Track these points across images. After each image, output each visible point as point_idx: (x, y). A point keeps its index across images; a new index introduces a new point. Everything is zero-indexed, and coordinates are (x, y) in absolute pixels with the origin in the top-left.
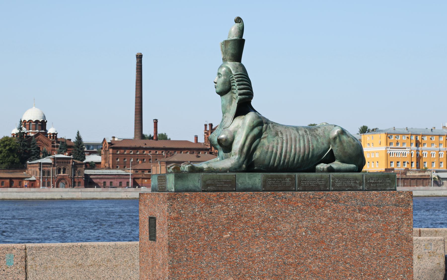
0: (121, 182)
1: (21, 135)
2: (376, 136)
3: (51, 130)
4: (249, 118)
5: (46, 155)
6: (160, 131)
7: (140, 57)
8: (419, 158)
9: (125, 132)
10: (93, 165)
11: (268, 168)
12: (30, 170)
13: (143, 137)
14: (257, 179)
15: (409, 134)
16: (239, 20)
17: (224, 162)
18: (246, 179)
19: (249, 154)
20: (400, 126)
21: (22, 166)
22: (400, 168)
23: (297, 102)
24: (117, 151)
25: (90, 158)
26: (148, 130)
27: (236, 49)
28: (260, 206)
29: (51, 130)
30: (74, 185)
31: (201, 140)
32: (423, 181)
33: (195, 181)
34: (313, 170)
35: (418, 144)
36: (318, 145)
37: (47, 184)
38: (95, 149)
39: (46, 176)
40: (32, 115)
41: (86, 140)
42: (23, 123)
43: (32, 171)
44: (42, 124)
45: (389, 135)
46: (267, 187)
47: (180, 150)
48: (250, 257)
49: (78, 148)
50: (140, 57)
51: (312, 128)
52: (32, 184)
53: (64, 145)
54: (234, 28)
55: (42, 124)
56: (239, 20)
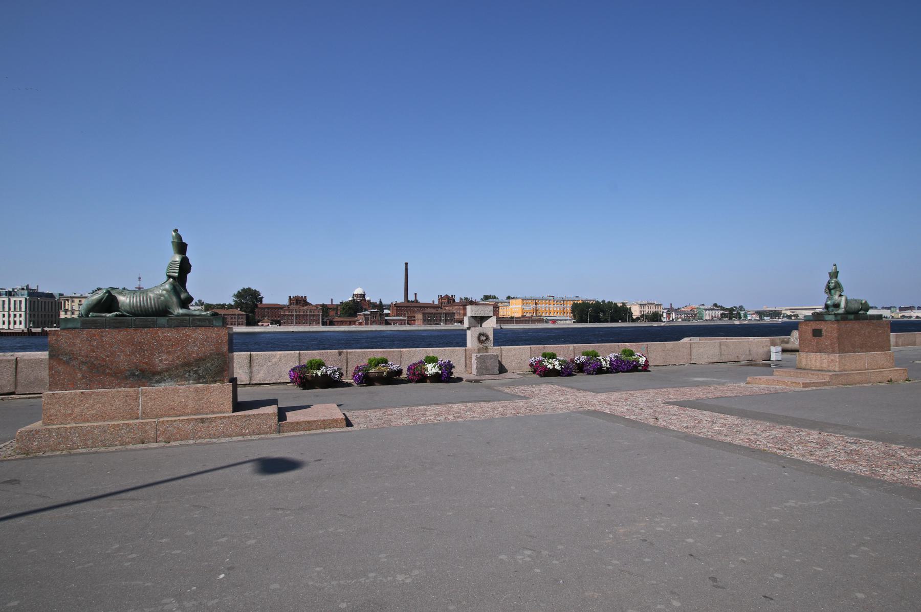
0: (402, 322)
1: (353, 301)
2: (517, 301)
3: (367, 299)
4: (843, 299)
5: (366, 310)
6: (411, 298)
7: (406, 264)
8: (537, 310)
9: (401, 299)
10: (387, 315)
12: (359, 317)
13: (408, 301)
15: (533, 299)
17: (841, 311)
20: (528, 296)
21: (355, 315)
22: (528, 315)
23: (853, 292)
24: (398, 308)
25: (386, 311)
26: (411, 298)
27: (834, 275)
29: (367, 299)
30: (380, 324)
31: (436, 302)
32: (540, 321)
33: (839, 317)
37: (367, 324)
38: (389, 307)
39: (293, 318)
40: (358, 291)
41: (384, 303)
42: (354, 295)
43: (360, 318)
44: (363, 296)
45: (523, 300)
47: (674, 334)
49: (381, 306)
50: (406, 264)
52: (360, 324)
53: (374, 305)
55: (363, 296)
56: (176, 231)
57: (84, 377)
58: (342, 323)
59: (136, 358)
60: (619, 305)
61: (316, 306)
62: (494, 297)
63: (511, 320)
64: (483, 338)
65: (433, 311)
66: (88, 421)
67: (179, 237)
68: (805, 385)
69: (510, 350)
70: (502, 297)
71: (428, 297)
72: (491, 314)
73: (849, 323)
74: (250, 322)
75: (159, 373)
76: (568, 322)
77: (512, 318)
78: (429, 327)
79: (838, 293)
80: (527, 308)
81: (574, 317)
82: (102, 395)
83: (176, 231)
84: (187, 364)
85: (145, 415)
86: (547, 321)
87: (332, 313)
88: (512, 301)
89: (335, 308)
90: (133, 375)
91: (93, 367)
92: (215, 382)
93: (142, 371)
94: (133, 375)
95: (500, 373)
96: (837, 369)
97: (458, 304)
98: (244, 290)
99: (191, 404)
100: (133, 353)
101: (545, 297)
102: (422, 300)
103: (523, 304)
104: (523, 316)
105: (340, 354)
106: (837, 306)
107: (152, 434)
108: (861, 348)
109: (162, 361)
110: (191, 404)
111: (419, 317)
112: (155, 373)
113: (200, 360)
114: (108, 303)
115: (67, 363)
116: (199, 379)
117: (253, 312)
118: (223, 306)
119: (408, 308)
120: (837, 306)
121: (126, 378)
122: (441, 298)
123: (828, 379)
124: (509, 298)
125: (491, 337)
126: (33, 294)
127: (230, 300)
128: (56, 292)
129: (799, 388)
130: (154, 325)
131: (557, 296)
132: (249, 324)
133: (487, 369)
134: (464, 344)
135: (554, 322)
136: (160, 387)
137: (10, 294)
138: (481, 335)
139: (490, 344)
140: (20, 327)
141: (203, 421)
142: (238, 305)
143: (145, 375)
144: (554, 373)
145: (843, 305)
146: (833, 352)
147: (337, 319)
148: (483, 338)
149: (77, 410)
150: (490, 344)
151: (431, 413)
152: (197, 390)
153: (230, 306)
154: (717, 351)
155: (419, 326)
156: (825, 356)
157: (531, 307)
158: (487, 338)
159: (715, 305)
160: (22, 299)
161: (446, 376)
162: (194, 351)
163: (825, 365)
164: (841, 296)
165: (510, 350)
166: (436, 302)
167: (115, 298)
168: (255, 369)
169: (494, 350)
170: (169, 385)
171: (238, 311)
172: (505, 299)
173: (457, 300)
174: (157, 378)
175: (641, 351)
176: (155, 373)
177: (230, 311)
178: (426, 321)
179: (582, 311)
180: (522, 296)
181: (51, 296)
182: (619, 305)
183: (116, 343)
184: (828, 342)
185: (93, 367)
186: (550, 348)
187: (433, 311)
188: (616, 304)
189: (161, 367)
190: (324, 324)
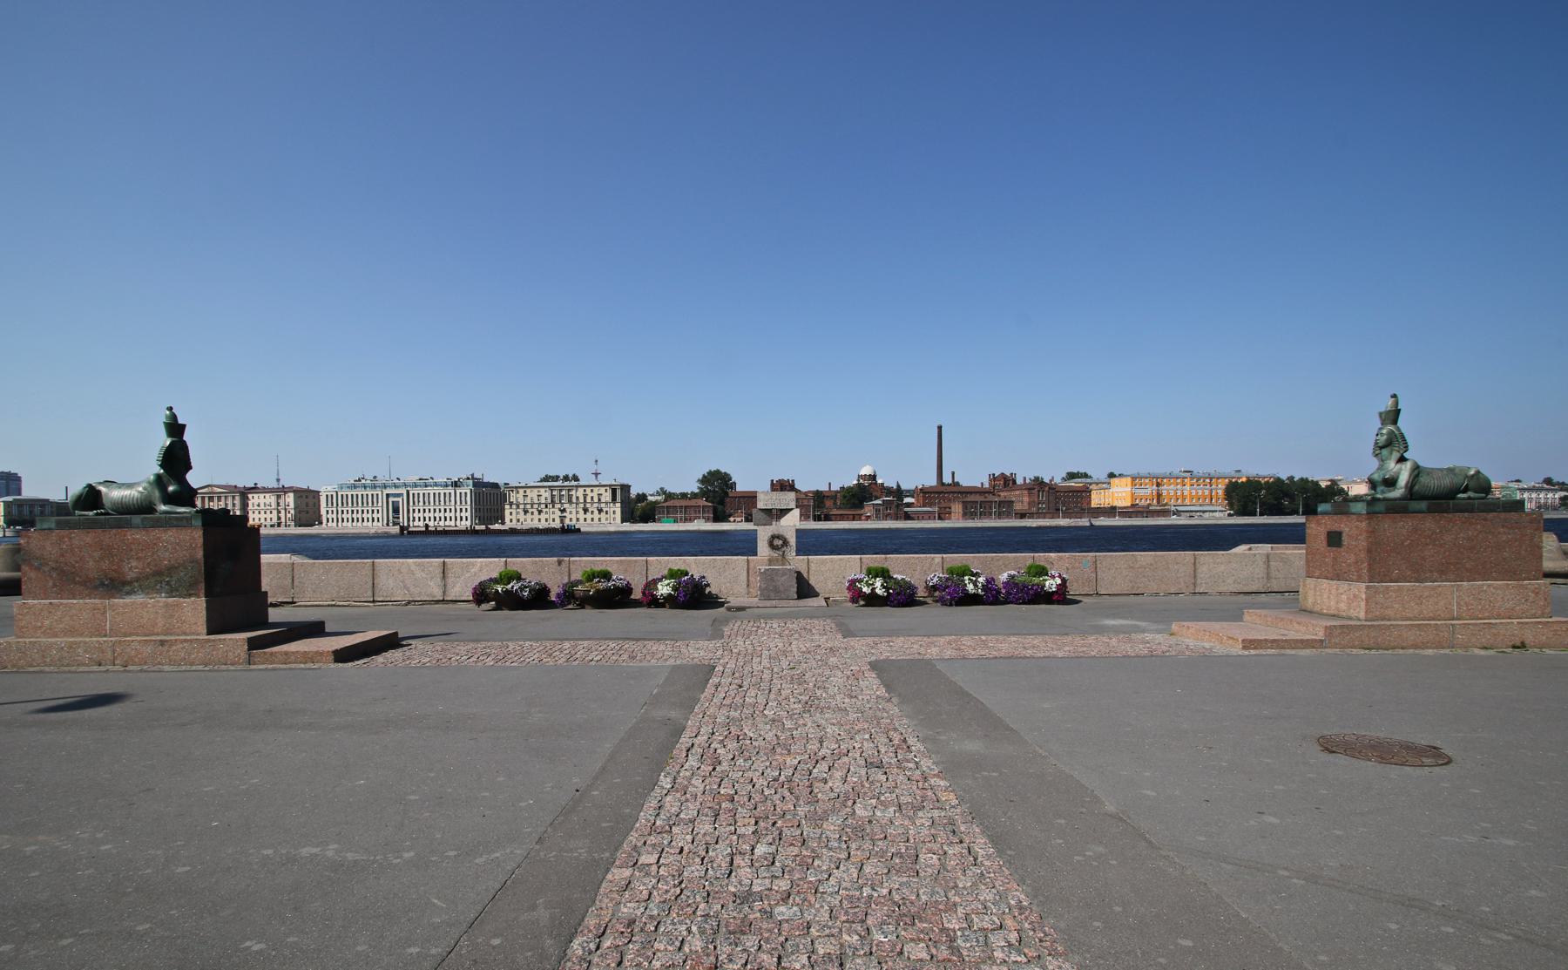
0: (929, 516)
1: (859, 485)
4: (1408, 465)
6: (947, 479)
7: (940, 428)
8: (1159, 495)
9: (932, 481)
10: (909, 505)
11: (1423, 498)
14: (1423, 505)
15: (1151, 477)
16: (1394, 396)
17: (1397, 493)
18: (1415, 505)
19: (1410, 486)
20: (1143, 472)
21: (862, 507)
22: (1143, 503)
23: (1436, 450)
24: (925, 494)
25: (907, 500)
26: (947, 479)
27: (1393, 416)
28: (1430, 523)
30: (897, 518)
31: (987, 485)
32: (1165, 513)
33: (1380, 507)
34: (1454, 498)
35: (1158, 485)
36: (1457, 480)
38: (911, 493)
40: (866, 471)
43: (868, 510)
44: (873, 477)
45: (1134, 478)
46: (1430, 510)
48: (1423, 558)
49: (899, 493)
50: (940, 428)
51: (1451, 470)
52: (868, 518)
53: (889, 491)
54: (1391, 402)
55: (873, 477)
56: (170, 409)
57: (55, 585)
58: (842, 518)
59: (105, 565)
60: (1323, 485)
61: (806, 494)
62: (1086, 476)
63: (1111, 511)
64: (778, 542)
65: (979, 498)
66: (56, 636)
67: (174, 417)
68: (1248, 644)
69: (823, 562)
70: (1098, 474)
71: (973, 476)
72: (793, 505)
73: (1441, 514)
74: (719, 518)
75: (130, 583)
76: (1220, 515)
77: (1114, 508)
78: (628, 527)
79: (1396, 455)
80: (1141, 492)
81: (1231, 506)
82: (126, 605)
83: (170, 409)
84: (159, 573)
85: (113, 633)
86: (1177, 513)
87: (828, 503)
88: (1113, 481)
89: (832, 496)
90: (103, 584)
91: (62, 573)
92: (190, 595)
93: (112, 580)
94: (103, 584)
95: (800, 597)
96: (1362, 615)
97: (1020, 488)
98: (710, 473)
99: (161, 622)
100: (102, 558)
101: (1176, 472)
102: (966, 481)
103: (1133, 485)
104: (1133, 506)
105: (560, 563)
106: (1391, 483)
107: (109, 655)
108: (1442, 573)
109: (132, 569)
110: (161, 622)
111: (957, 508)
112: (124, 583)
113: (171, 569)
114: (91, 498)
115: (38, 569)
116: (172, 592)
117: (722, 502)
118: (684, 496)
119: (942, 495)
120: (1391, 483)
121: (96, 588)
122: (993, 478)
123: (1321, 635)
124: (1112, 475)
125: (793, 541)
126: (478, 484)
127: (693, 487)
128: (501, 482)
129: (1237, 650)
130: (129, 525)
131: (1199, 470)
132: (717, 519)
133: (776, 590)
134: (753, 551)
135: (1191, 514)
136: (128, 600)
137: (456, 485)
138: (774, 537)
139: (791, 553)
140: (465, 524)
141: (162, 643)
142: (703, 493)
143: (114, 585)
144: (973, 600)
145: (1403, 479)
146: (1359, 579)
147: (835, 512)
148: (778, 542)
149: (47, 622)
150: (791, 553)
151: (591, 652)
152: (167, 605)
153: (694, 496)
154: (1260, 570)
155: (956, 522)
156: (1344, 586)
157: (1148, 490)
158: (786, 543)
159: (1548, 481)
160: (467, 490)
161: (694, 596)
162: (166, 558)
163: (1343, 606)
164: (1402, 459)
165: (823, 562)
166: (987, 485)
167: (99, 492)
168: (450, 581)
169: (797, 562)
170: (139, 599)
171: (702, 502)
172: (1103, 477)
173: (1019, 481)
174: (128, 588)
175: (1059, 568)
176: (124, 583)
177: (693, 502)
178: (967, 514)
179: (1243, 495)
180: (1134, 472)
181: (496, 486)
182: (1323, 485)
183: (83, 544)
184: (1352, 559)
185: (62, 573)
186: (1041, 558)
187: (979, 498)
188: (1316, 484)
189: (131, 575)
190: (817, 518)
